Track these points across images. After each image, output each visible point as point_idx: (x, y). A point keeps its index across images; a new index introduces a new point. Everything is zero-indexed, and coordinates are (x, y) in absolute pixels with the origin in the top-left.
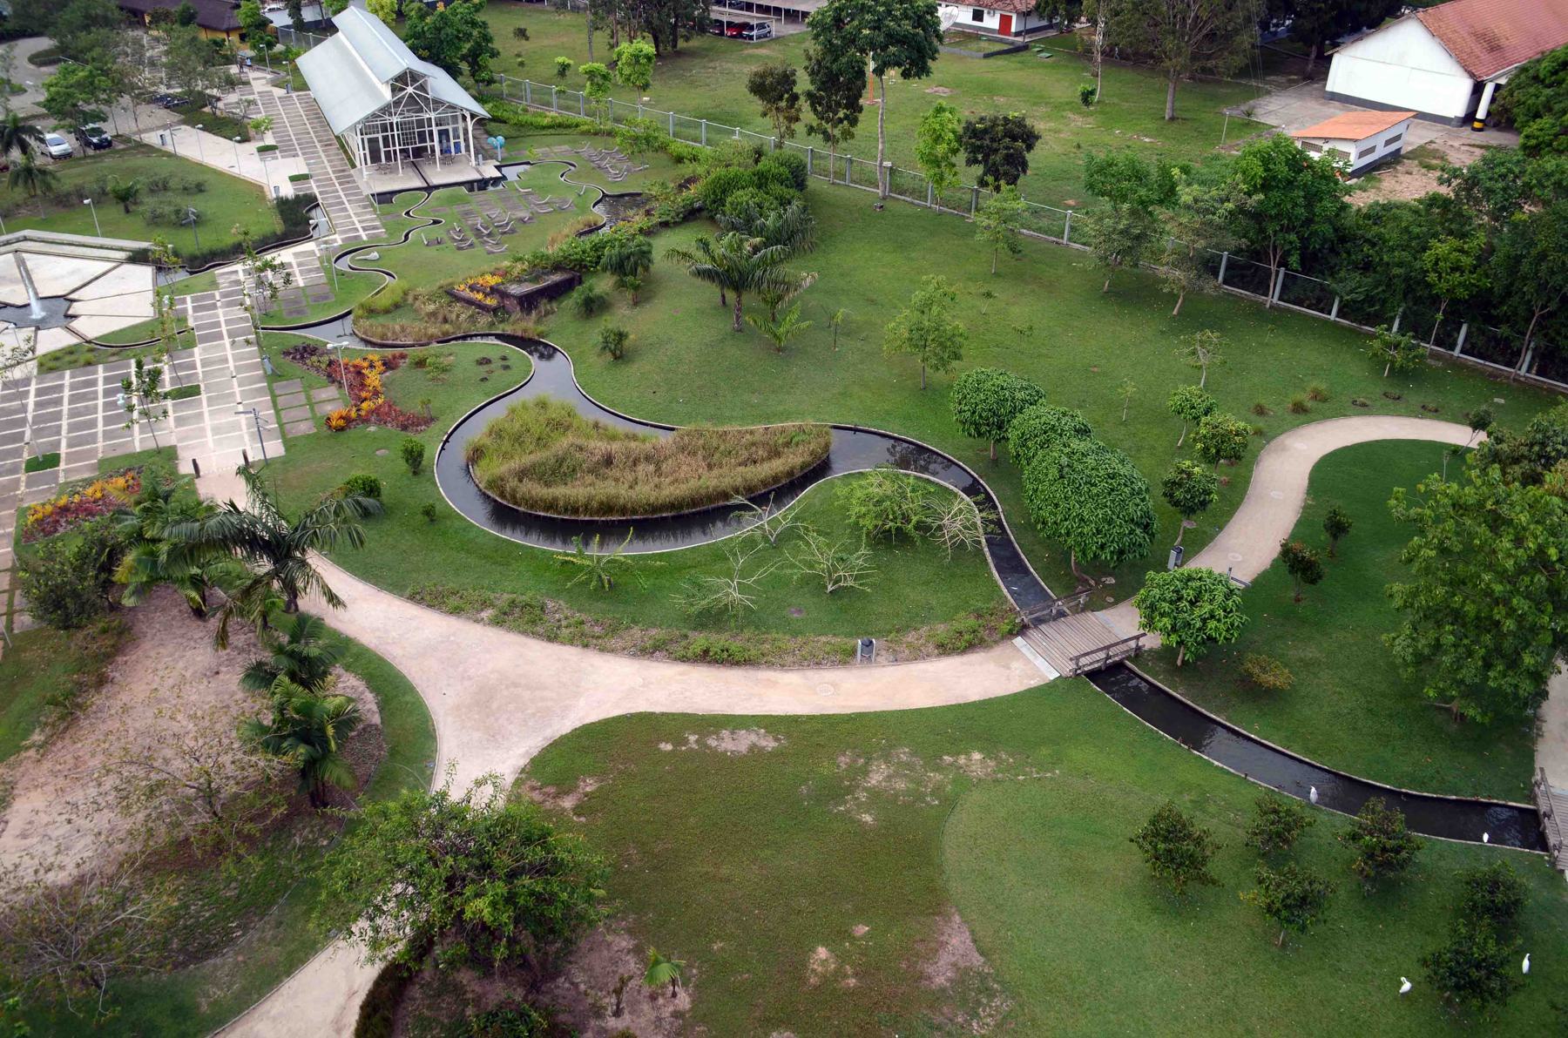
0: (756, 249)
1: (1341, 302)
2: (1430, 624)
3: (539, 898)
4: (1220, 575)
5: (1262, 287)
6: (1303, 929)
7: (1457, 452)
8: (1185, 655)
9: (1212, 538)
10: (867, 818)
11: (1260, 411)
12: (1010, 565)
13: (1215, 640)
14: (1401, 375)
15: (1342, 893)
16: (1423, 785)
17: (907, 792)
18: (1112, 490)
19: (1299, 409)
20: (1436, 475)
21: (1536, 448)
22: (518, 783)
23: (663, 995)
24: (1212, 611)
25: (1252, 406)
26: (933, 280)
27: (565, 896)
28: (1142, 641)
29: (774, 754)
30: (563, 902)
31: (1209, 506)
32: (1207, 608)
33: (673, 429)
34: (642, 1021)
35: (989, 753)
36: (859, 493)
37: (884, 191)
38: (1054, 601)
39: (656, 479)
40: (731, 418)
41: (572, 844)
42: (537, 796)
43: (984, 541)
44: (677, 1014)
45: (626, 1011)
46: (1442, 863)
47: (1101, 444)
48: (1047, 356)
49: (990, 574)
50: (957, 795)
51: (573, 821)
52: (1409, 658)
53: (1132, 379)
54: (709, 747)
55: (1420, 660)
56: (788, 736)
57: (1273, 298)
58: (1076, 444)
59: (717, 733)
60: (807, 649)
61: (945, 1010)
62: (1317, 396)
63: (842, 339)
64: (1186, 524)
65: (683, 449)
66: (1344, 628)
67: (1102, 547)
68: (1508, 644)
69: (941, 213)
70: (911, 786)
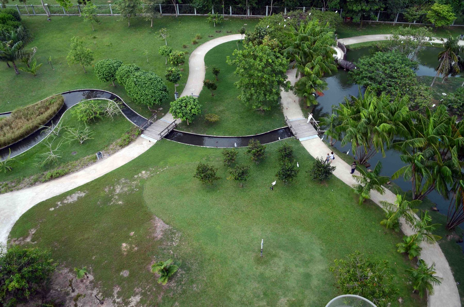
0: (12, 45)
1: (196, 9)
2: (248, 89)
3: (32, 272)
4: (190, 96)
5: (174, 11)
6: (245, 180)
7: (240, 42)
8: (189, 122)
9: (184, 87)
10: (120, 202)
11: (185, 47)
12: (131, 115)
13: (195, 114)
14: (219, 25)
15: (251, 167)
16: (261, 131)
17: (128, 191)
18: (152, 83)
19: (195, 43)
20: (236, 50)
21: (258, 35)
22: (9, 242)
23: (84, 279)
24: (192, 107)
25: (182, 46)
26: (75, 39)
27: (40, 267)
28: (176, 122)
29: (85, 197)
30: (40, 269)
31: (180, 78)
32: (190, 107)
33: (10, 113)
34: (82, 289)
35: (146, 170)
36: (78, 111)
37: (49, 14)
38: (148, 120)
39: (11, 130)
40: (28, 103)
41: (33, 251)
42: (17, 243)
43: (121, 111)
44: (91, 282)
45: (76, 289)
46: (272, 149)
47: (144, 71)
48: (119, 51)
49: (127, 120)
50: (143, 185)
51: (33, 244)
52: (245, 100)
53: (146, 49)
54: (65, 203)
55: (248, 100)
56: (88, 190)
57: (178, 14)
58: (137, 74)
59: (66, 198)
60: (82, 163)
61: (164, 243)
62: (199, 38)
63: (54, 66)
64: (176, 85)
65: (16, 118)
66: (227, 98)
67: (155, 100)
68: (268, 88)
69: (70, 16)
70: (129, 188)
